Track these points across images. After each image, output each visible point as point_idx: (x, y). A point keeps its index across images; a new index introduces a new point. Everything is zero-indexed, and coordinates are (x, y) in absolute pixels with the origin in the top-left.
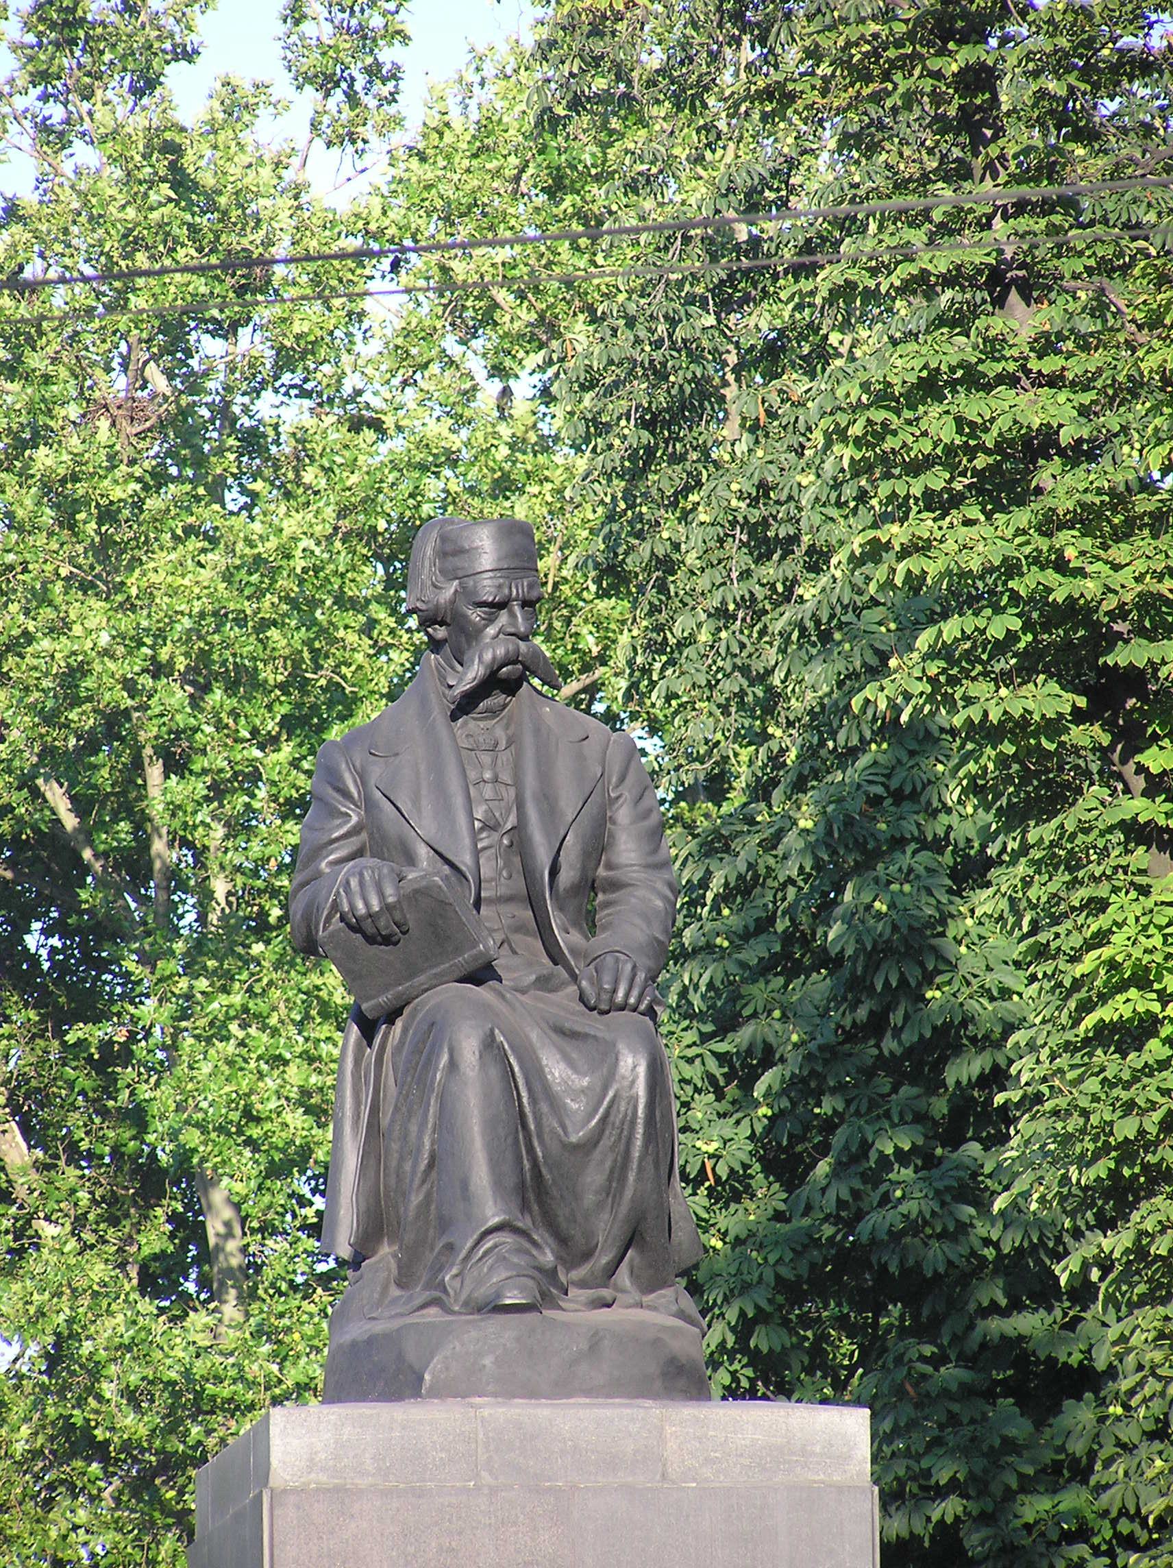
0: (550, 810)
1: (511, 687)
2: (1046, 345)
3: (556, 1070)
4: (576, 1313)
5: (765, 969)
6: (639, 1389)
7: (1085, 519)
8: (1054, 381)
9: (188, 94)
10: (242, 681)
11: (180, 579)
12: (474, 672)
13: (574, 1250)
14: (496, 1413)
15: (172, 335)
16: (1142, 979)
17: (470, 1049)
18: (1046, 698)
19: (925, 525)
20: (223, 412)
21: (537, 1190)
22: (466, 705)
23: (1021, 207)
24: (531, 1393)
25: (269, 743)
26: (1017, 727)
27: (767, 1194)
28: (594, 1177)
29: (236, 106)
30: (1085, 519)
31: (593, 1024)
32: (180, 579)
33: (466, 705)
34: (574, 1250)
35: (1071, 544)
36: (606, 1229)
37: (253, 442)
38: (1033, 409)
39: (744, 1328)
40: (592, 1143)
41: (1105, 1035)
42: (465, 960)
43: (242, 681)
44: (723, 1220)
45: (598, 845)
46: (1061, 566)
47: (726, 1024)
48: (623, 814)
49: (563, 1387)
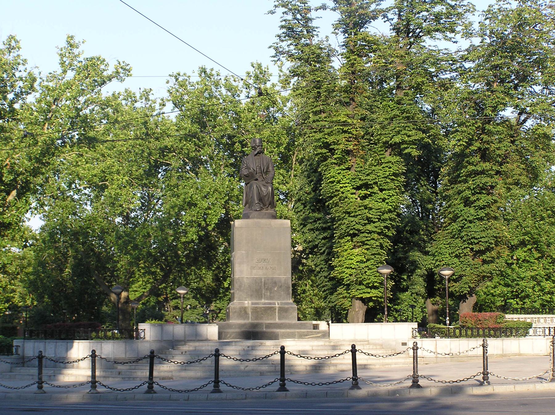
0: (263, 165)
1: (260, 153)
2: (325, 118)
3: (263, 189)
4: (264, 211)
5: (313, 172)
6: (268, 218)
7: (328, 134)
8: (326, 121)
9: (269, 85)
10: (272, 142)
11: (266, 133)
12: (256, 152)
13: (264, 205)
14: (256, 220)
15: (268, 108)
16: (333, 177)
17: (255, 187)
18: (324, 151)
19: (314, 134)
20: (273, 115)
21: (261, 200)
22: (256, 155)
23: (323, 105)
24: (259, 218)
25: (275, 148)
26: (321, 153)
27: (313, 194)
28: (266, 199)
29: (274, 85)
30: (328, 134)
31: (267, 184)
32: (266, 133)
33: (256, 155)
34: (264, 205)
35: (326, 136)
36: (267, 203)
37: (275, 118)
38: (323, 123)
39: (310, 207)
40: (265, 196)
41: (330, 182)
42: (255, 178)
43: (272, 142)
44: (308, 196)
45: (268, 168)
46: (326, 139)
47: (309, 178)
48: (270, 165)
49: (262, 218)
